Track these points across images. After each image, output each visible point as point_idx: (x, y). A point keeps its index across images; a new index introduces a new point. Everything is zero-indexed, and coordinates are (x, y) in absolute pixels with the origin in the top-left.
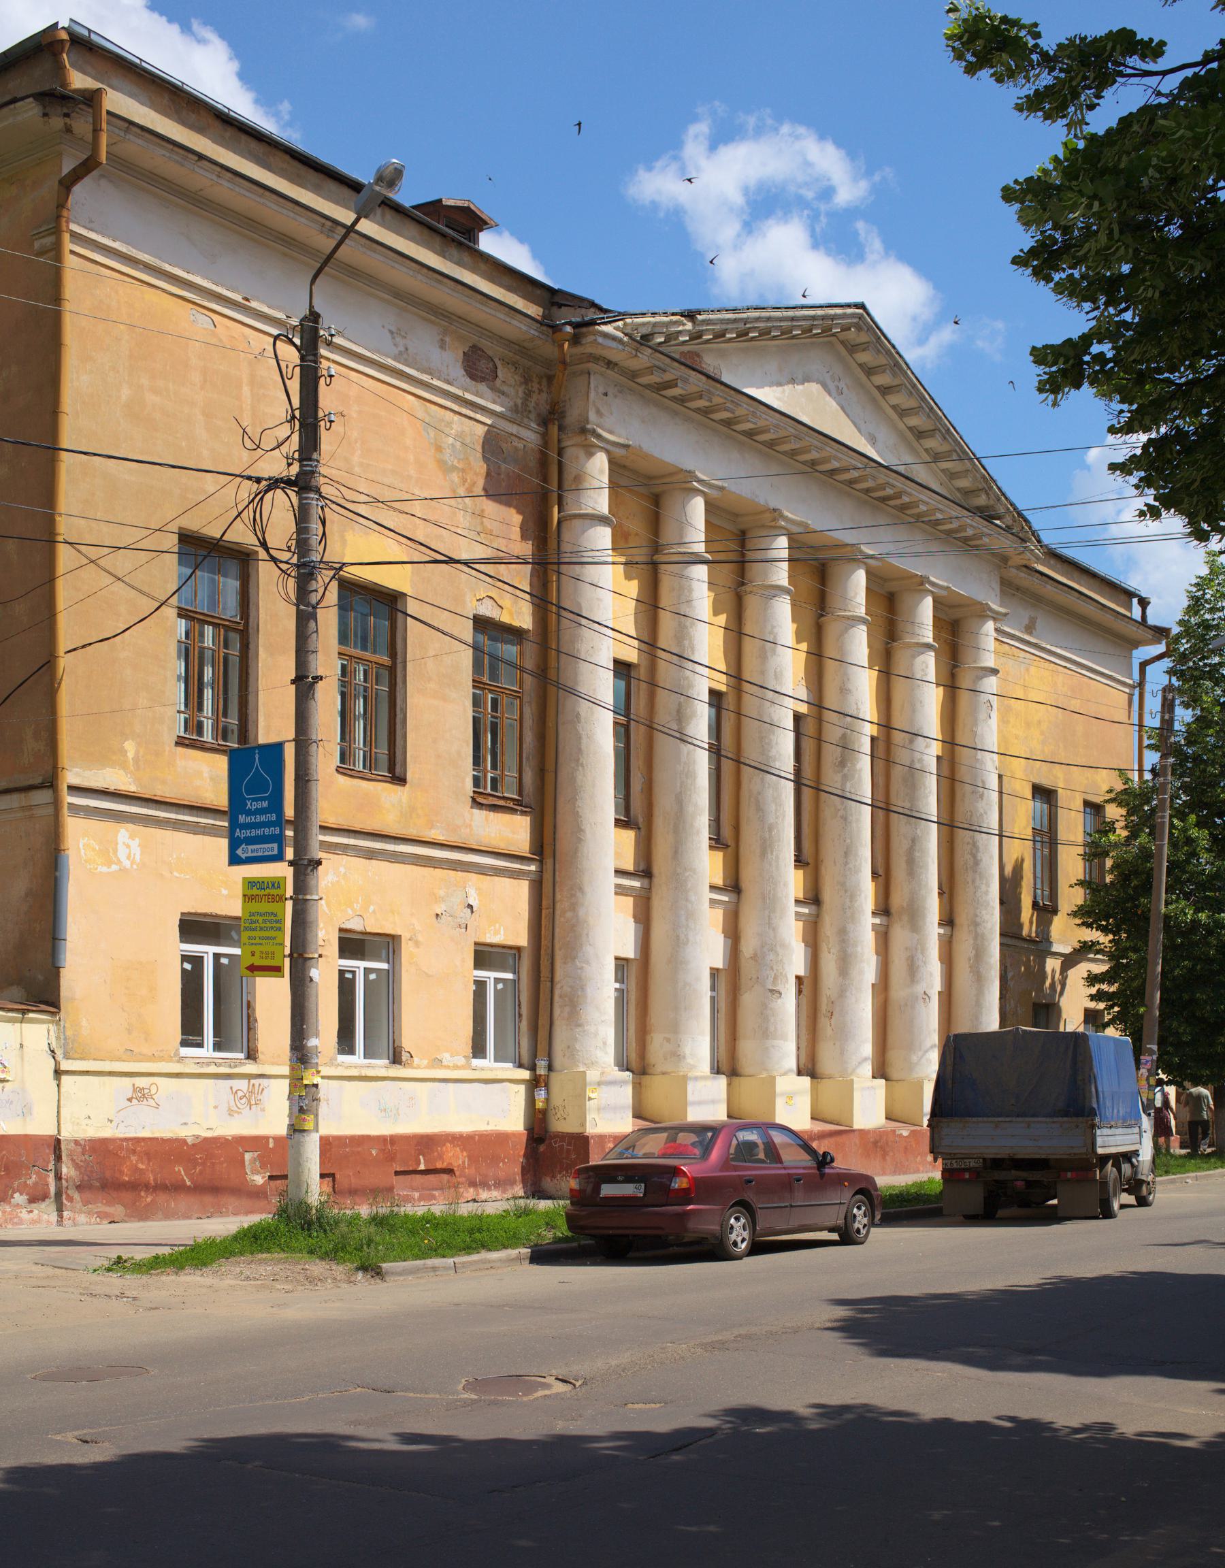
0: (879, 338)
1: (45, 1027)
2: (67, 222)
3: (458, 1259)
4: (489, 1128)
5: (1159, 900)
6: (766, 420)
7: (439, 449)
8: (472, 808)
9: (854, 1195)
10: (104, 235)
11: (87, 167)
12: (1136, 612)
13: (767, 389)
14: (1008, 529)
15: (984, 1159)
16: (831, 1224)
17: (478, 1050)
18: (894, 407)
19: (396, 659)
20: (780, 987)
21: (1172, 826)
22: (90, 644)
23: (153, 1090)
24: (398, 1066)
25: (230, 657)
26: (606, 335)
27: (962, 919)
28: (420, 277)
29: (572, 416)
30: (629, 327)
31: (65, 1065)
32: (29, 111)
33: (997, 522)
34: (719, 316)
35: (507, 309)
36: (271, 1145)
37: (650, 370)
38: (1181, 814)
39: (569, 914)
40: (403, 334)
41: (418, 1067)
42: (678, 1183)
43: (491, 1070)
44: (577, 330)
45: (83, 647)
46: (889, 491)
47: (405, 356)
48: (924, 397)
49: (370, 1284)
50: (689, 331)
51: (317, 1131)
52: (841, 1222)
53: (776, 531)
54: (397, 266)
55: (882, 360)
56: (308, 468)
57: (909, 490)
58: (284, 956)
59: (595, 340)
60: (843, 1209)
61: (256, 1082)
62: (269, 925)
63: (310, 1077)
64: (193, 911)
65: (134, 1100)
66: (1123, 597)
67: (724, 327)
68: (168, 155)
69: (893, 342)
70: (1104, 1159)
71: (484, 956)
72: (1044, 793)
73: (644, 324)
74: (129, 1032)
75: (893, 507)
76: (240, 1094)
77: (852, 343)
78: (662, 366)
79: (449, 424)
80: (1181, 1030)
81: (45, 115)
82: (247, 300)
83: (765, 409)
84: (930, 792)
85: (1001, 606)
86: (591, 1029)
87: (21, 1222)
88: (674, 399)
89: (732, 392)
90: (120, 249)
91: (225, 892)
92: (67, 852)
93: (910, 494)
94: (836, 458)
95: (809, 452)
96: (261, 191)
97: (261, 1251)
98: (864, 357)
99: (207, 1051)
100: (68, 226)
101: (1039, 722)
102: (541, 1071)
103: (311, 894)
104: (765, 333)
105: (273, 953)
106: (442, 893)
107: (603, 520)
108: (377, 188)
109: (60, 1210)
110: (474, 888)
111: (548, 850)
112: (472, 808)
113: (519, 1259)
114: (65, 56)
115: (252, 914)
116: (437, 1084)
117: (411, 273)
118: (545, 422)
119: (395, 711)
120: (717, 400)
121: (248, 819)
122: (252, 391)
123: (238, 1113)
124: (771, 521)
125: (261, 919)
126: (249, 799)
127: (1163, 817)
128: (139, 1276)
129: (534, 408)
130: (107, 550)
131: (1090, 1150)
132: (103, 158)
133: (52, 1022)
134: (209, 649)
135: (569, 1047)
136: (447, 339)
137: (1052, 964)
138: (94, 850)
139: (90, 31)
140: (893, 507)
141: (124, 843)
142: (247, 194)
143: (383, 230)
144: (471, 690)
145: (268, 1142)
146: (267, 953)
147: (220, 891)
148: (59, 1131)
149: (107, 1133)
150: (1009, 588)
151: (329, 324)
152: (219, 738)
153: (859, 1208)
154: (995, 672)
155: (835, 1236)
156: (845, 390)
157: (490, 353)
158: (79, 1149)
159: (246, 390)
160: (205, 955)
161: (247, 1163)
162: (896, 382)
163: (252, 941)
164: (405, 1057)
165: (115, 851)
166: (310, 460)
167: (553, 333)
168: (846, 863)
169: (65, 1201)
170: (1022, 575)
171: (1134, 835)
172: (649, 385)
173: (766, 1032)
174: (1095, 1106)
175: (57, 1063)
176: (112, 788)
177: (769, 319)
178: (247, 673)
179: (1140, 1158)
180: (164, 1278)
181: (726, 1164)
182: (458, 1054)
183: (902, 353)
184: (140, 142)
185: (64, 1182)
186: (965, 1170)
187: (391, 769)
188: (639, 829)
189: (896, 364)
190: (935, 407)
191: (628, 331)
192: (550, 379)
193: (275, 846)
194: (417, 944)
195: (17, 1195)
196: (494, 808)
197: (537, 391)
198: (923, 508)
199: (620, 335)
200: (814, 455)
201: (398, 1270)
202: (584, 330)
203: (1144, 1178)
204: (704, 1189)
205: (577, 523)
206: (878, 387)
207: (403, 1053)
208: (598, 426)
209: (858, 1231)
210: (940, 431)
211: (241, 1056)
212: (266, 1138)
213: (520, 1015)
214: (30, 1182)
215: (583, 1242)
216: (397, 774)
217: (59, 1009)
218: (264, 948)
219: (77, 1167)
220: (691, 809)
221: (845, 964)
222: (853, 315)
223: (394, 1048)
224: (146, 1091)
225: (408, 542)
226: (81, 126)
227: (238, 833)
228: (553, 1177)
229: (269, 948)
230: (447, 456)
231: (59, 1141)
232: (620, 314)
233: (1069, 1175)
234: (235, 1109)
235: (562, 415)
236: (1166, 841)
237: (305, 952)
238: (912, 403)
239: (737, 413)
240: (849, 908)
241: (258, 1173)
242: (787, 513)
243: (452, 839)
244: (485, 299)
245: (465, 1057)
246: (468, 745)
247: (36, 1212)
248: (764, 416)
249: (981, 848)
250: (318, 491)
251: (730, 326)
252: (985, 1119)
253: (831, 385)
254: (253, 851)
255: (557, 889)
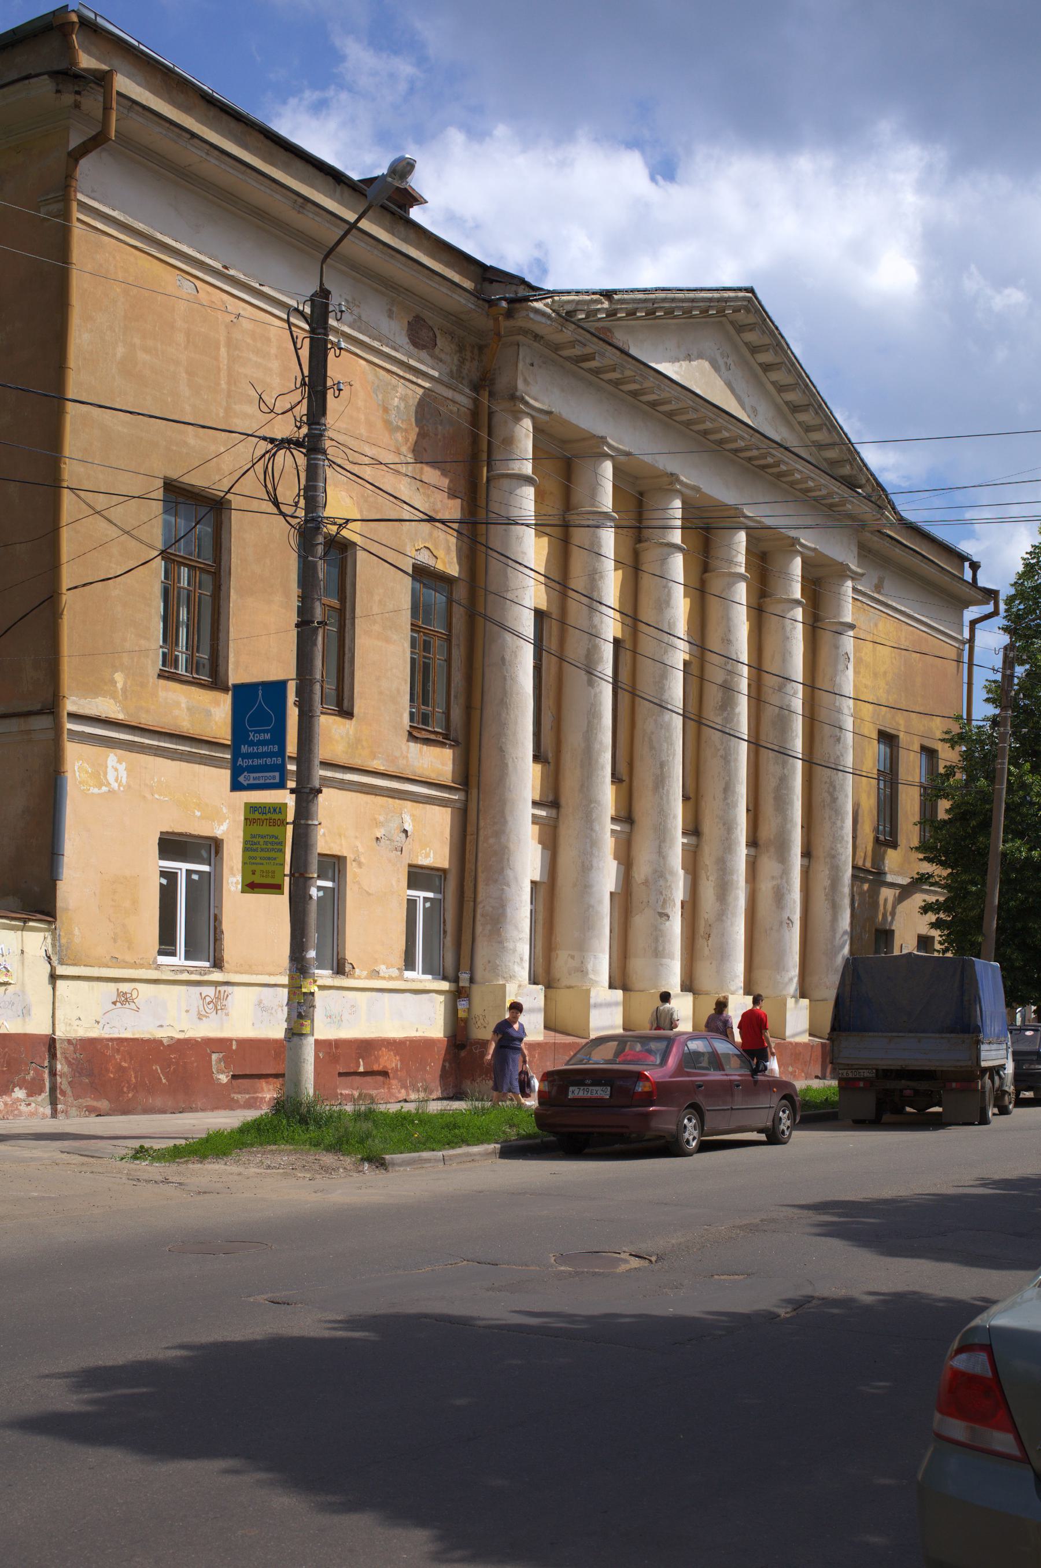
0: (765, 320)
1: (42, 934)
2: (75, 192)
3: (445, 1153)
4: (418, 1034)
5: (998, 838)
6: (668, 392)
7: (386, 410)
8: (408, 741)
9: (781, 1100)
10: (105, 204)
11: (96, 141)
12: (968, 575)
13: (664, 364)
14: (868, 498)
15: (877, 1070)
16: (761, 1125)
17: (409, 963)
18: (773, 383)
19: (345, 602)
20: (668, 911)
21: (1010, 773)
22: (91, 583)
23: (135, 995)
24: (342, 977)
25: (202, 596)
26: (537, 311)
27: (819, 852)
28: (376, 252)
29: (502, 382)
30: (556, 305)
31: (60, 970)
32: (44, 87)
33: (860, 491)
34: (631, 296)
35: (449, 284)
36: (234, 1047)
37: (572, 344)
38: (1014, 761)
39: (492, 841)
40: (357, 303)
41: (359, 978)
42: (640, 1087)
43: (421, 981)
44: (512, 305)
45: (84, 585)
46: (770, 460)
47: (359, 324)
48: (801, 374)
49: (376, 1174)
50: (606, 309)
51: (313, 1035)
52: (769, 1124)
53: (672, 492)
54: (357, 241)
55: (767, 340)
56: (316, 432)
57: (786, 460)
58: (285, 875)
59: (528, 315)
60: (772, 1112)
61: (222, 989)
62: (269, 846)
63: (308, 986)
64: (170, 830)
65: (118, 1004)
66: (957, 561)
67: (635, 306)
68: (165, 132)
69: (776, 323)
70: (985, 1070)
71: (418, 876)
72: (887, 738)
73: (569, 302)
74: (115, 940)
75: (771, 474)
76: (208, 999)
77: (741, 323)
78: (583, 341)
79: (395, 388)
80: (1014, 956)
81: (58, 91)
82: (226, 267)
83: (669, 382)
84: (796, 735)
85: (858, 567)
86: (510, 945)
87: (20, 1114)
88: (590, 371)
89: (642, 366)
90: (118, 217)
91: (198, 814)
92: (66, 774)
93: (787, 464)
94: (727, 429)
95: (704, 422)
96: (243, 168)
97: (269, 1143)
98: (751, 337)
99: (178, 960)
100: (76, 196)
101: (885, 673)
102: (464, 982)
103: (312, 820)
104: (669, 312)
105: (274, 872)
106: (381, 818)
107: (527, 480)
108: (389, 179)
109: (53, 1102)
110: (409, 815)
111: (473, 780)
112: (408, 741)
113: (487, 1155)
114: (74, 36)
115: (253, 836)
116: (374, 994)
117: (369, 248)
118: (476, 388)
119: (344, 651)
120: (628, 373)
121: (250, 750)
122: (228, 352)
123: (206, 1017)
124: (668, 484)
125: (262, 841)
126: (252, 731)
127: (1003, 763)
128: (167, 1164)
129: (467, 374)
130: (115, 499)
131: (975, 1064)
132: (113, 135)
133: (48, 930)
134: (184, 588)
135: (489, 962)
136: (394, 309)
137: (887, 894)
138: (87, 772)
139: (96, 15)
140: (771, 474)
141: (113, 767)
142: (231, 171)
143: (341, 207)
144: (409, 633)
145: (231, 1045)
146: (267, 872)
147: (194, 813)
148: (54, 1031)
149: (94, 1033)
150: (865, 552)
151: (336, 300)
152: (194, 671)
153: (784, 1112)
154: (852, 627)
155: (763, 1137)
156: (732, 367)
157: (431, 323)
158: (72, 1048)
159: (223, 351)
160: (179, 871)
161: (214, 1063)
162: (778, 360)
163: (254, 861)
164: (348, 968)
165: (105, 774)
166: (318, 424)
167: (490, 307)
168: (725, 799)
169: (59, 1096)
170: (876, 539)
171: (971, 779)
172: (569, 357)
173: (582, 947)
174: (980, 1024)
175: (53, 968)
176: (103, 716)
177: (673, 300)
178: (219, 613)
179: (1006, 1072)
180: (191, 1166)
181: (679, 1071)
182: (392, 966)
183: (784, 335)
184: (140, 119)
185: (58, 1078)
186: (860, 1079)
187: (339, 702)
188: (549, 763)
189: (779, 344)
190: (810, 384)
191: (556, 307)
192: (481, 348)
193: (277, 774)
194: (360, 865)
195: (17, 1089)
196: (427, 742)
197: (469, 359)
198: (798, 476)
199: (549, 311)
200: (708, 425)
201: (398, 1161)
202: (518, 305)
203: (1006, 1089)
204: (663, 1092)
205: (505, 483)
206: (760, 364)
207: (346, 964)
208: (526, 394)
209: (783, 1132)
210: (813, 405)
211: (207, 964)
212: (230, 1040)
213: (445, 932)
214: (28, 1077)
215: (545, 1139)
216: (345, 709)
217: (56, 919)
218: (265, 868)
219: (69, 1064)
220: (597, 746)
221: (724, 889)
222: (744, 298)
223: (338, 960)
224: (129, 995)
225: (391, 499)
226: (92, 103)
227: (240, 762)
228: (473, 1080)
229: (270, 868)
230: (393, 417)
231: (54, 1040)
232: (549, 292)
233: (954, 1085)
234: (203, 1013)
235: (493, 382)
236: (1005, 786)
237: (306, 872)
238: (789, 380)
239: (645, 385)
240: (727, 839)
241: (223, 1072)
242: (682, 478)
243: (391, 769)
244: (430, 274)
245: (398, 969)
246: (406, 683)
247: (33, 1105)
248: (667, 389)
249: (838, 787)
250: (324, 452)
251: (640, 306)
252: (880, 1034)
253: (721, 362)
254: (254, 779)
255: (481, 817)
